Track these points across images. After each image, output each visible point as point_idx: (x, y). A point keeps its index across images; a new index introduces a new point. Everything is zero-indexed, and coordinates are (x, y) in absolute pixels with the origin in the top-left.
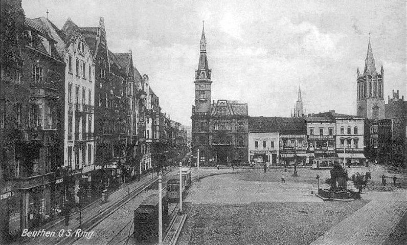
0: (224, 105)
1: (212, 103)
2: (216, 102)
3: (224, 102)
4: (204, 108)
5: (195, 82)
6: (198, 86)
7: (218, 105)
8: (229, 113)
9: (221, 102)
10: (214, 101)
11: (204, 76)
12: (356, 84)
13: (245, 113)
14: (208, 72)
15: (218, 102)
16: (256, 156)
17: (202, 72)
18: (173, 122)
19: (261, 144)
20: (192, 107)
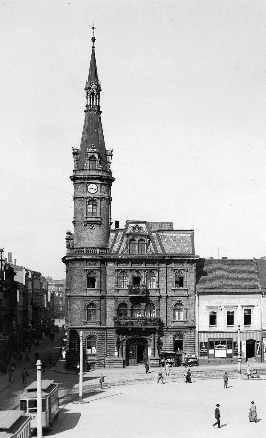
0: (143, 233)
1: (113, 227)
2: (122, 226)
3: (140, 225)
4: (91, 239)
5: (73, 179)
6: (80, 188)
7: (128, 232)
8: (170, 246)
9: (134, 225)
10: (117, 223)
11: (94, 165)
12: (30, 393)
13: (187, 250)
14: (104, 157)
15: (127, 226)
16: (212, 344)
17: (89, 155)
18: (21, 268)
19: (222, 319)
20: (65, 236)
